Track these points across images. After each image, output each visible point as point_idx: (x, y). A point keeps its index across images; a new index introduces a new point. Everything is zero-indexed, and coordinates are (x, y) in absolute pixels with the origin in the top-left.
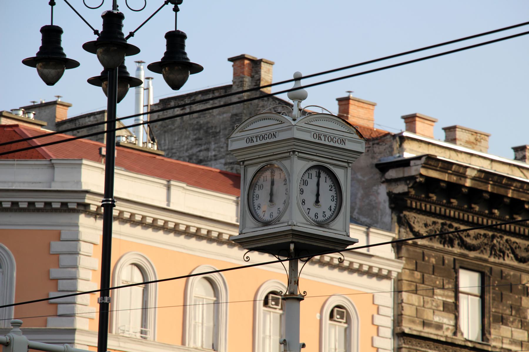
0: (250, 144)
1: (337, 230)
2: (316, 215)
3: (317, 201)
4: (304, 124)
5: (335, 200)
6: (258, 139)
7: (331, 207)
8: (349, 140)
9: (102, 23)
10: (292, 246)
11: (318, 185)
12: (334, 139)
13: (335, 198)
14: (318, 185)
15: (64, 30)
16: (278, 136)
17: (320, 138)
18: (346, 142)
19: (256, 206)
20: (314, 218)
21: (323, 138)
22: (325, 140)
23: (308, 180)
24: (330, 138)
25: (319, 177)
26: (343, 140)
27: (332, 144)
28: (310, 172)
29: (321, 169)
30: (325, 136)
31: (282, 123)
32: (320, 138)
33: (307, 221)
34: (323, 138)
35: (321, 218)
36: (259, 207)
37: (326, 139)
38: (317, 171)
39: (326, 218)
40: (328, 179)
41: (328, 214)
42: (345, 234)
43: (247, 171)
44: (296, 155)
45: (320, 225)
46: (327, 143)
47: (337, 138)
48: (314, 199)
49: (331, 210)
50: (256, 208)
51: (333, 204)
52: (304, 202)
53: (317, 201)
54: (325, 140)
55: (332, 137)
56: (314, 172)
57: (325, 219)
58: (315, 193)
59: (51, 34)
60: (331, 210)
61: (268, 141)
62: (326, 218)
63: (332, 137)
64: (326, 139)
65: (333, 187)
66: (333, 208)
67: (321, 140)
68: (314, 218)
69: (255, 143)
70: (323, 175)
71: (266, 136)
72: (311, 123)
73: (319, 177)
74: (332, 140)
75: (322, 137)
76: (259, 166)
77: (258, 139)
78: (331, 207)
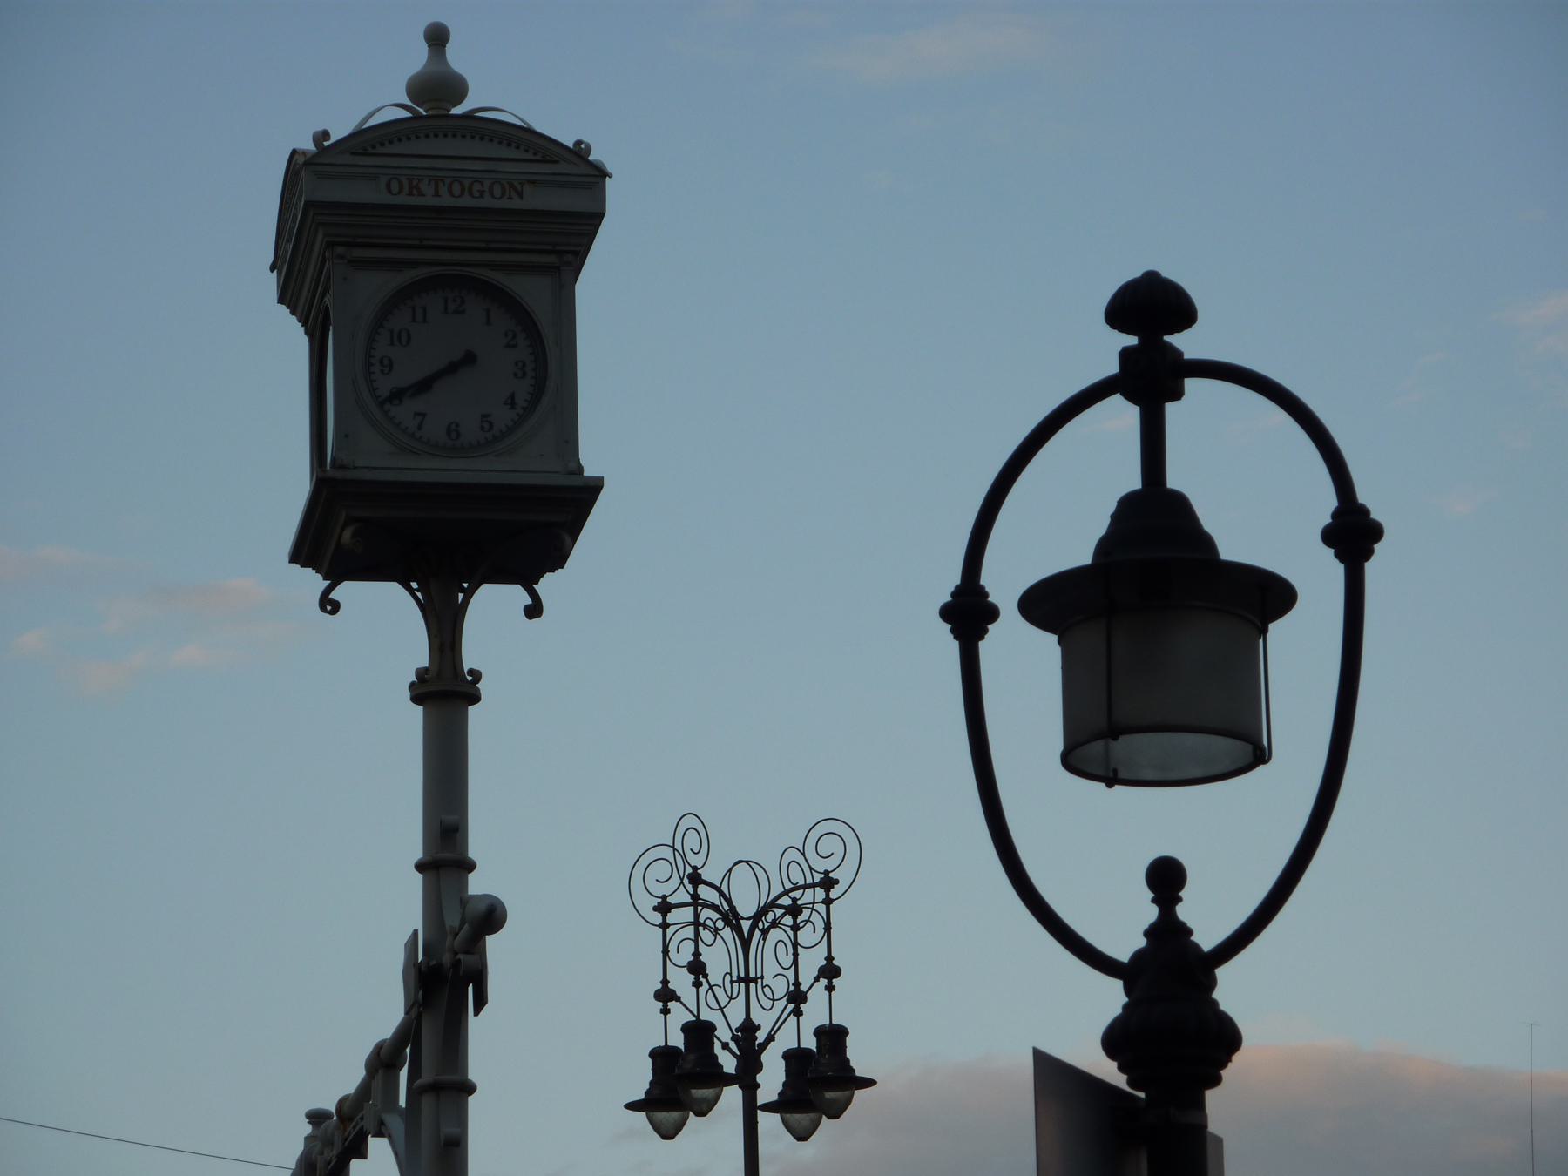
7: (512, 397)
12: (477, 187)
22: (437, 194)
26: (512, 186)
37: (443, 190)
44: (342, 257)
47: (487, 183)
49: (513, 405)
54: (437, 194)
55: (467, 183)
60: (513, 405)
63: (467, 183)
64: (443, 190)
67: (421, 194)
78: (512, 397)
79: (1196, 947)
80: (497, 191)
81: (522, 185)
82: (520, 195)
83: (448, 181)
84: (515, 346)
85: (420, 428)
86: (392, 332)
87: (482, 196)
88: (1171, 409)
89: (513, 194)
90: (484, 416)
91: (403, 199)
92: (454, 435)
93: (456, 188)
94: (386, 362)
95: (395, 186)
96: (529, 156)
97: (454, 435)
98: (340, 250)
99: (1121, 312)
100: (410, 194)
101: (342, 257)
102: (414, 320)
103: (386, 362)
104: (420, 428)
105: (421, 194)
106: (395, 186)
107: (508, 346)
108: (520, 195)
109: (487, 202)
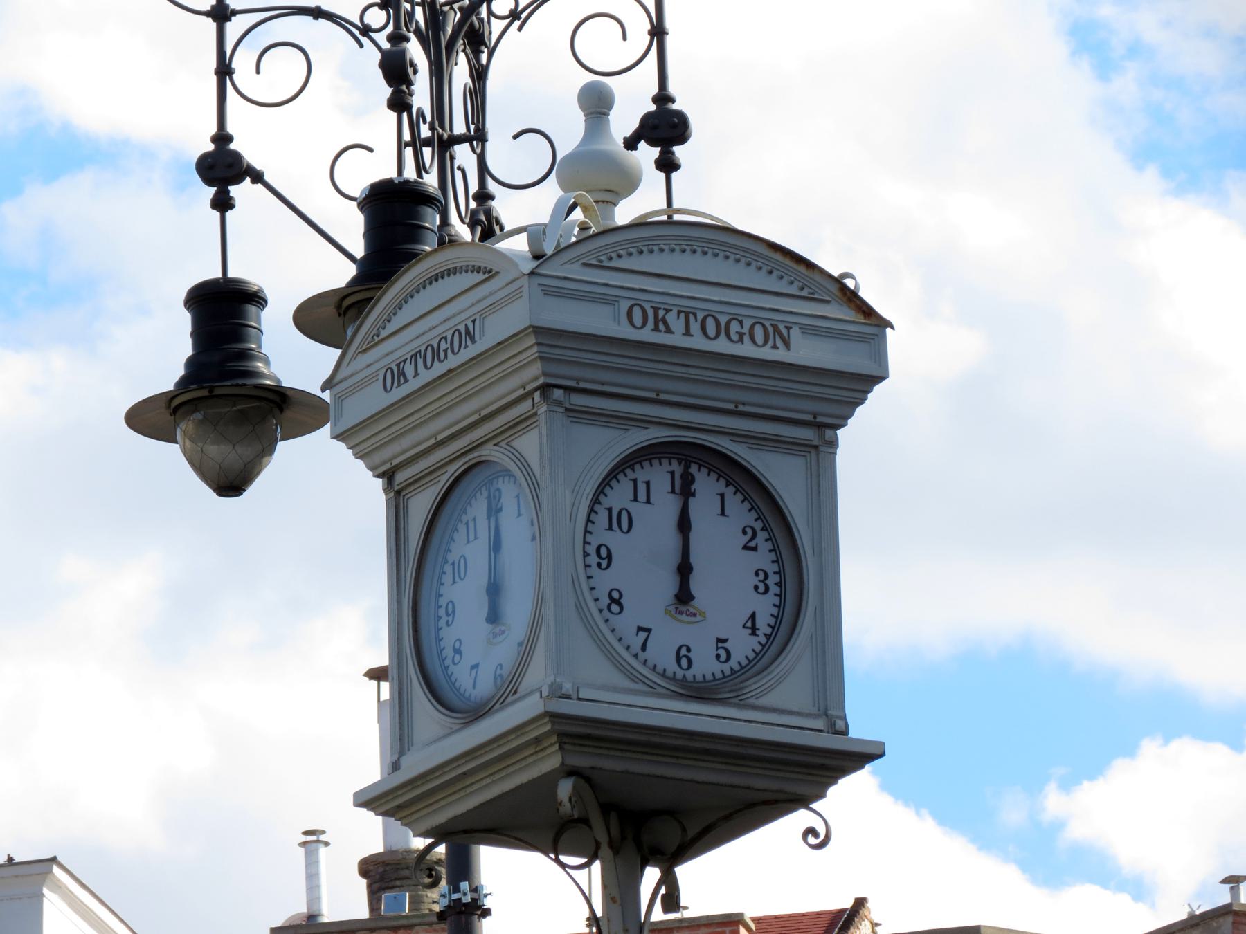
0: (399, 393)
1: (791, 713)
2: (682, 655)
3: (684, 596)
4: (577, 266)
5: (774, 589)
6: (420, 362)
7: (753, 617)
8: (807, 330)
9: (362, 230)
10: (565, 789)
11: (684, 525)
12: (735, 327)
13: (773, 579)
14: (684, 525)
15: (269, 294)
16: (482, 333)
17: (660, 323)
18: (795, 334)
19: (448, 652)
20: (672, 667)
21: (677, 324)
22: (687, 333)
23: (635, 508)
24: (710, 324)
25: (685, 490)
26: (777, 330)
27: (722, 346)
28: (641, 474)
29: (689, 458)
30: (687, 315)
31: (491, 274)
32: (660, 323)
33: (634, 679)
34: (677, 324)
35: (705, 665)
36: (458, 651)
37: (695, 327)
38: (677, 468)
39: (733, 663)
40: (734, 502)
41: (743, 646)
42: (819, 724)
43: (406, 508)
44: (558, 403)
45: (700, 692)
46: (697, 342)
47: (747, 323)
48: (668, 585)
49: (754, 631)
50: (448, 662)
51: (765, 607)
52: (618, 602)
53: (684, 596)
54: (687, 333)
55: (723, 320)
56: (659, 476)
57: (726, 668)
58: (674, 559)
59: (222, 310)
60: (754, 631)
61: (453, 361)
62: (733, 663)
63: (723, 320)
64: (695, 327)
65: (762, 536)
66: (763, 624)
67: (668, 330)
68: (672, 667)
69: (413, 384)
70: (707, 486)
71: (443, 346)
72: (613, 264)
73: (685, 490)
74: (723, 330)
75: (671, 318)
76: (445, 479)
77: (420, 362)
78: (753, 617)
79: (654, 865)
80: (759, 337)
81: (788, 328)
82: (787, 344)
83: (700, 316)
84: (754, 549)
85: (644, 648)
86: (610, 510)
87: (741, 340)
88: (228, 24)
89: (779, 343)
90: (719, 640)
91: (647, 335)
92: (684, 662)
93: (711, 330)
94: (604, 552)
95: (638, 319)
96: (793, 290)
97: (684, 662)
98: (558, 394)
99: (635, 148)
100: (656, 329)
101: (558, 403)
102: (636, 499)
103: (604, 552)
104: (644, 648)
105: (668, 330)
106: (638, 319)
107: (746, 547)
108: (787, 344)
109: (746, 349)
